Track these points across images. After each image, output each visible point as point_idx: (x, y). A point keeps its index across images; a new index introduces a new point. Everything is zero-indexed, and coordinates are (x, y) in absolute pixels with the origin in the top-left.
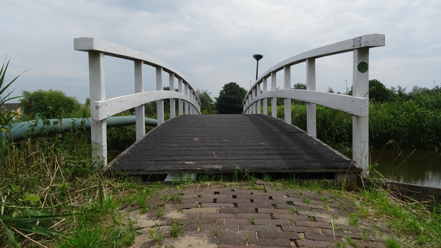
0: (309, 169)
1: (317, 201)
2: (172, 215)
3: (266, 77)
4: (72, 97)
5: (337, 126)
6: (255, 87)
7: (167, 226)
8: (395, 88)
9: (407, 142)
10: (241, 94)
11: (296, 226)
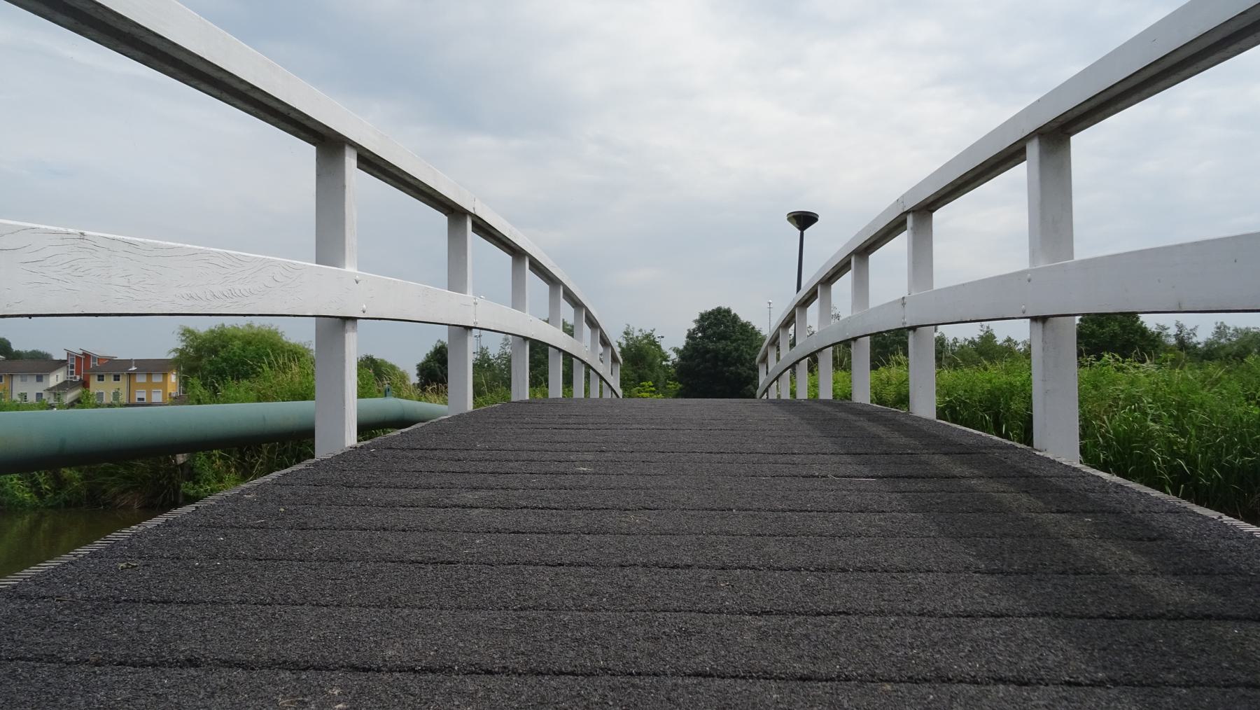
3: (829, 280)
4: (303, 342)
6: (789, 321)
8: (1169, 328)
10: (743, 340)
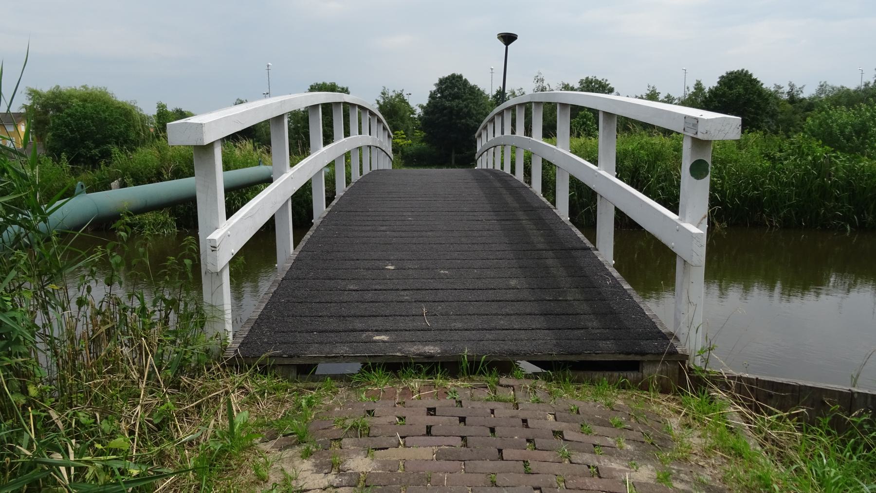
0: (594, 355)
1: (604, 428)
2: (356, 465)
5: (660, 183)
7: (349, 488)
8: (783, 87)
9: (794, 215)
10: (471, 99)
11: (567, 488)
